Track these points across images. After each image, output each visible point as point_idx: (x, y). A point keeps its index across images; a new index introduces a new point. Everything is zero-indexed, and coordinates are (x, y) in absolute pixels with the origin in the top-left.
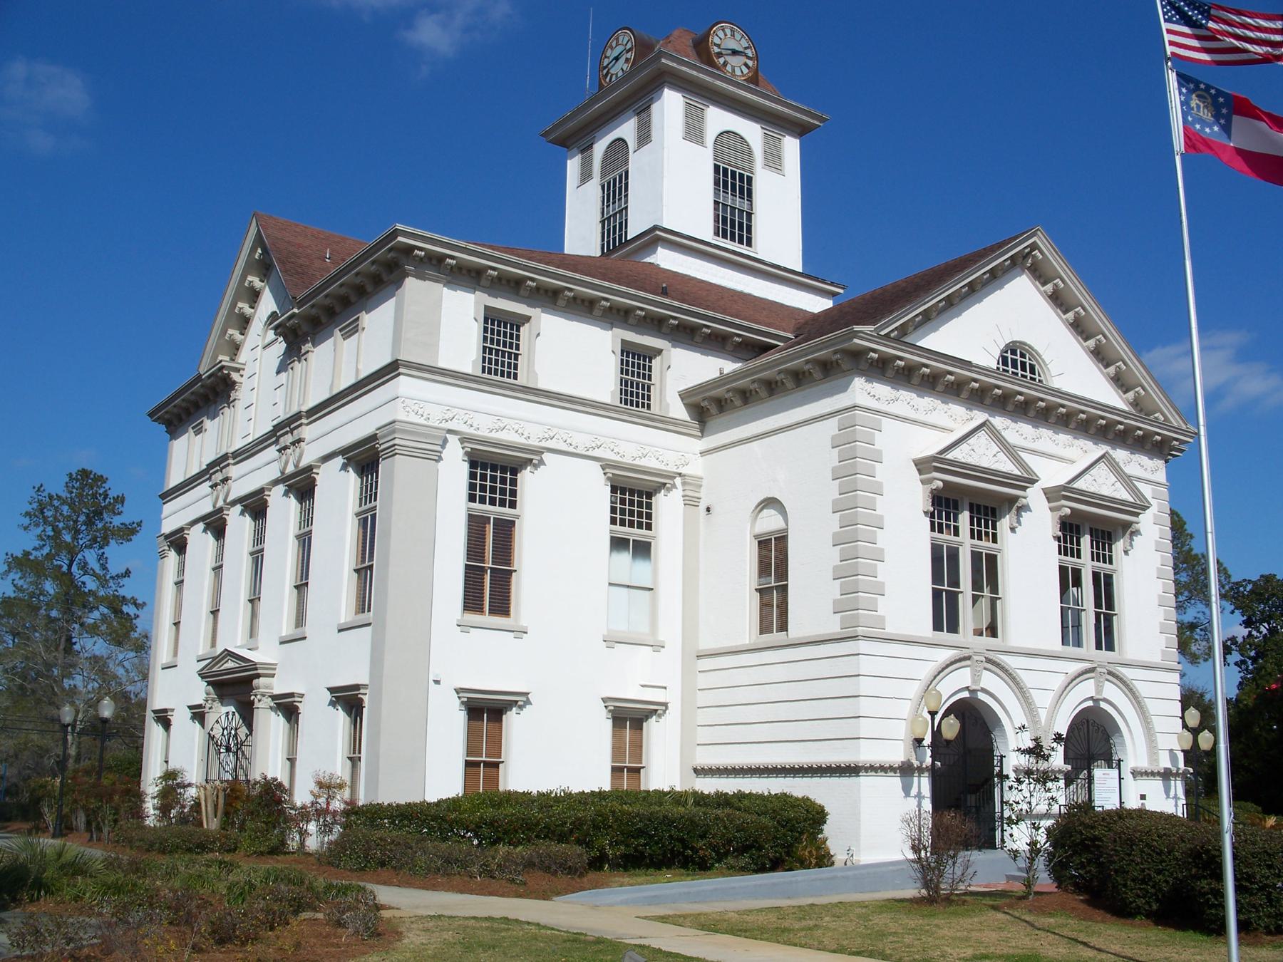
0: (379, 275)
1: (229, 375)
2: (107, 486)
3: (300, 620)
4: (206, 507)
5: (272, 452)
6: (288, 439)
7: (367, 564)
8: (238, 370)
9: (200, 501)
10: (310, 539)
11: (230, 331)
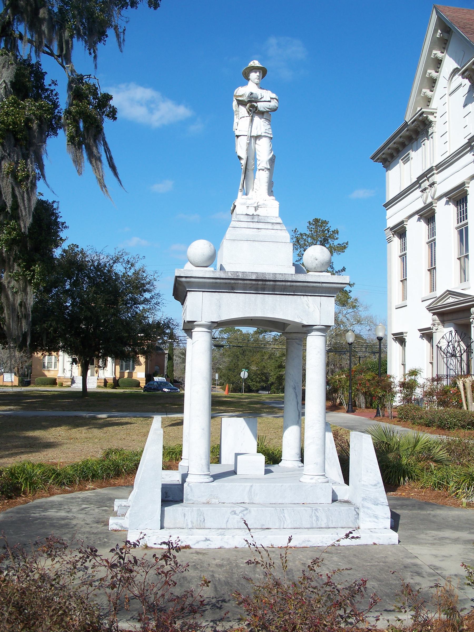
0: (411, 136)
1: (427, 117)
2: (329, 225)
3: (404, 297)
4: (420, 205)
5: (417, 193)
6: (426, 184)
7: (433, 267)
8: (432, 114)
9: (416, 201)
10: (435, 243)
11: (424, 90)
